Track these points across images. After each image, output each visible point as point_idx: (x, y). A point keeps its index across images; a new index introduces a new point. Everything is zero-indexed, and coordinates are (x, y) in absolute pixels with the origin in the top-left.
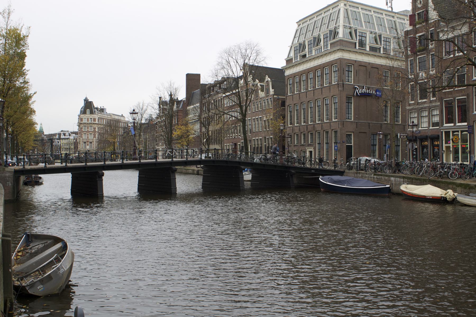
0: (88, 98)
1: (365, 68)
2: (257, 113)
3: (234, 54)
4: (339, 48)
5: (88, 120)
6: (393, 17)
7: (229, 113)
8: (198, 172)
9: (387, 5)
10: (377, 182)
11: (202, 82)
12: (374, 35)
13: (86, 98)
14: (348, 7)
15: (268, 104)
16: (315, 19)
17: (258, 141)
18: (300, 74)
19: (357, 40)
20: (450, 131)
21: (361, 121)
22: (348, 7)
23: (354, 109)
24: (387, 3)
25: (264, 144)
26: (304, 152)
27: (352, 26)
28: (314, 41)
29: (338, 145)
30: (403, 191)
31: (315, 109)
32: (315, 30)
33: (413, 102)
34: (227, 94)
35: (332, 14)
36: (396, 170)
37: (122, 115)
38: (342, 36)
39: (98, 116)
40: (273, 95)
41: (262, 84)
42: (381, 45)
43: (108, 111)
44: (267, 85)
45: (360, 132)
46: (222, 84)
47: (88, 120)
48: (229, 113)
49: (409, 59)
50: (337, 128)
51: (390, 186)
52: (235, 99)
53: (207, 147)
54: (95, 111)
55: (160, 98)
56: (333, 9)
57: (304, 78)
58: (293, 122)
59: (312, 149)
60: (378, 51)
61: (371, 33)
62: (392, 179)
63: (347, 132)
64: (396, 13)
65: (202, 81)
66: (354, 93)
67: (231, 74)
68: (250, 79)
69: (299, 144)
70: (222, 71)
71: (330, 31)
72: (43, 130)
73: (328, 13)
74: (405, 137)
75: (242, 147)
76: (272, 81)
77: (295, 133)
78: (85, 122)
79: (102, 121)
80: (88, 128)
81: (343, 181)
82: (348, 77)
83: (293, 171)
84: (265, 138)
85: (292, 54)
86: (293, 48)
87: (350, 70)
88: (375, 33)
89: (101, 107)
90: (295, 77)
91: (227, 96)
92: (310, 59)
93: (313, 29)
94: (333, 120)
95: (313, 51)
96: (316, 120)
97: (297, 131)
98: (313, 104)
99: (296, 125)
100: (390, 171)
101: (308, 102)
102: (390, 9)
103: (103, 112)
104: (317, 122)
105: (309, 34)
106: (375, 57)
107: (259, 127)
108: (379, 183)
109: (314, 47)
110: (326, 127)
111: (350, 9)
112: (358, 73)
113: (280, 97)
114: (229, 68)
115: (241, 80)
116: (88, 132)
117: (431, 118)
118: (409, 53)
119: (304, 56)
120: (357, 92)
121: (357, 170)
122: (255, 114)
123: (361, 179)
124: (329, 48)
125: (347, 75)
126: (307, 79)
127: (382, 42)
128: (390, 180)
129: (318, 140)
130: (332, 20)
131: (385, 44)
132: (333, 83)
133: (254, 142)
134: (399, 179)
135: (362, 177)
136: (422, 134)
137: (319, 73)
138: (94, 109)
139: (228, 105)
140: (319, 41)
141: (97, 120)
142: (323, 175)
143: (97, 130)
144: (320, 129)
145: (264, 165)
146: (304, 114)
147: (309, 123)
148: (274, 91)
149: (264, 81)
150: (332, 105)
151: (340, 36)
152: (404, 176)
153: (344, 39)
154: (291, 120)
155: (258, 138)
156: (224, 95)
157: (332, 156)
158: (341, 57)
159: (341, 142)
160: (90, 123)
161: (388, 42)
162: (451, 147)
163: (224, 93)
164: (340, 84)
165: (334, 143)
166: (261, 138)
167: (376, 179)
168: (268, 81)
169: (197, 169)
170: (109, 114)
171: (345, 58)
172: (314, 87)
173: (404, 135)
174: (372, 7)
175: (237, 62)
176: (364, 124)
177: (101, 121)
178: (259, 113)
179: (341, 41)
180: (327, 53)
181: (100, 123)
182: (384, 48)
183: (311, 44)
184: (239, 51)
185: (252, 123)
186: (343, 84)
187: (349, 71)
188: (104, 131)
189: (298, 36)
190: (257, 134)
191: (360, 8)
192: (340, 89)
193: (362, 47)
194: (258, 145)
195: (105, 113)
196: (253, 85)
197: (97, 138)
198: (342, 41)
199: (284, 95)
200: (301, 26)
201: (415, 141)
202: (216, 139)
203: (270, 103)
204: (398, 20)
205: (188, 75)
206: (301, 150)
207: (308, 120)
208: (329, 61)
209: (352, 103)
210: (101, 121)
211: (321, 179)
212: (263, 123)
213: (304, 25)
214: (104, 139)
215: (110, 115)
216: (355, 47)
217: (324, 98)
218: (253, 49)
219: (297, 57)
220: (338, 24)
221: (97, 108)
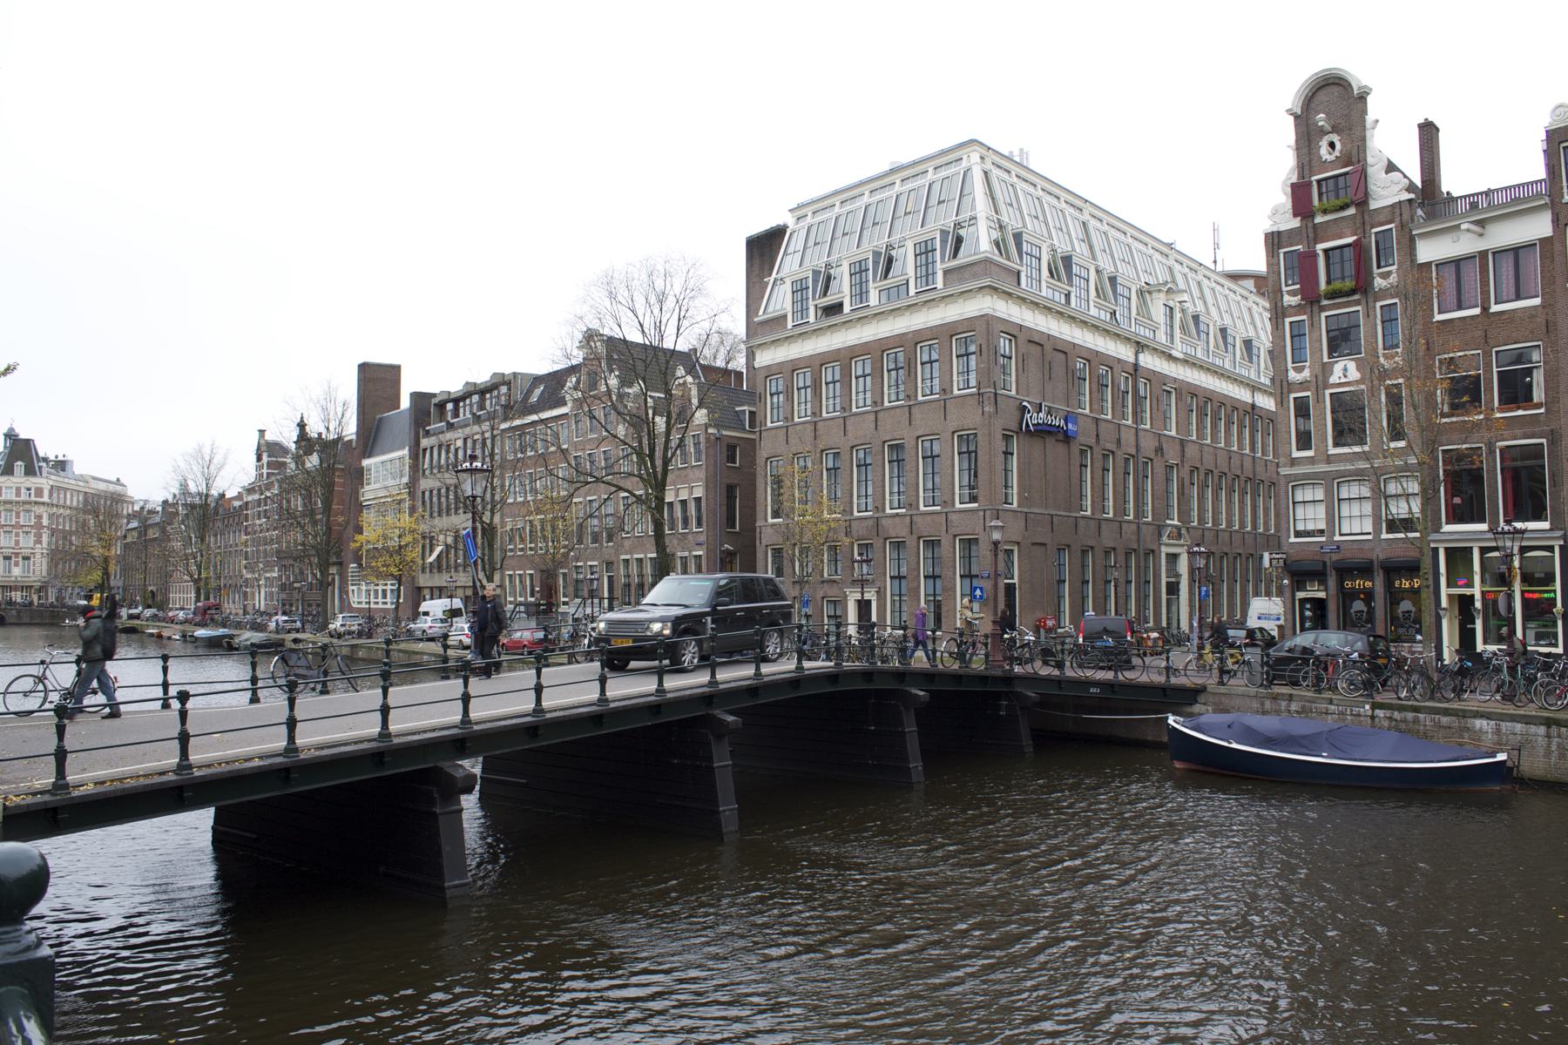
4: (986, 282)
5: (18, 493)
13: (12, 429)
18: (818, 363)
20: (1471, 548)
31: (880, 469)
37: (118, 480)
39: (51, 483)
40: (707, 426)
43: (79, 468)
47: (18, 493)
54: (40, 468)
55: (262, 432)
71: (942, 232)
74: (1281, 561)
79: (62, 496)
80: (18, 516)
81: (1304, 737)
89: (57, 457)
96: (884, 504)
103: (64, 470)
113: (725, 433)
116: (18, 526)
119: (836, 309)
124: (940, 285)
134: (1518, 727)
136: (1349, 555)
138: (38, 461)
143: (45, 522)
144: (904, 532)
152: (1548, 718)
155: (641, 556)
160: (25, 503)
162: (1478, 596)
170: (82, 476)
176: (1040, 517)
177: (59, 498)
181: (55, 502)
186: (996, 394)
188: (74, 526)
192: (987, 409)
195: (70, 475)
197: (45, 544)
201: (1319, 575)
205: (364, 368)
210: (59, 498)
214: (74, 548)
215: (82, 478)
221: (45, 460)
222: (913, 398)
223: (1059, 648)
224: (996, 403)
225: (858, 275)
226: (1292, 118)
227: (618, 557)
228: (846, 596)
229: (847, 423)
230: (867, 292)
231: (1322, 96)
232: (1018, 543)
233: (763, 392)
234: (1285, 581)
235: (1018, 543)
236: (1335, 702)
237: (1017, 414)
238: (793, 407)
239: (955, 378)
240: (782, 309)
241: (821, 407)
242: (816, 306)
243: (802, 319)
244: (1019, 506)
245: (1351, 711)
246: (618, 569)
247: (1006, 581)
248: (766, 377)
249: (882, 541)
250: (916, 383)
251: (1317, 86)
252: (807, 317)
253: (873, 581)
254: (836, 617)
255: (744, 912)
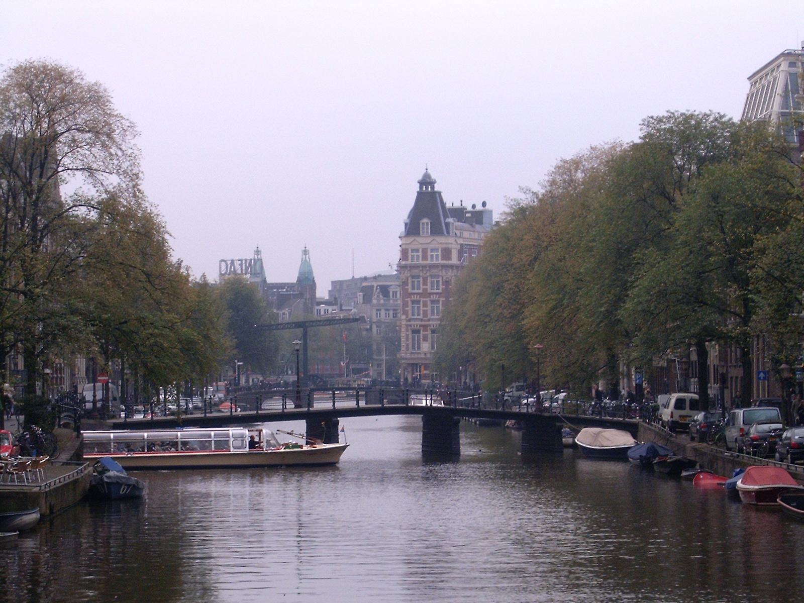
0: (433, 177)
5: (425, 257)
39: (460, 241)
47: (425, 257)
54: (447, 225)
72: (310, 272)
78: (415, 262)
89: (474, 206)
141: (454, 254)
223: (786, 293)
255: (682, 576)
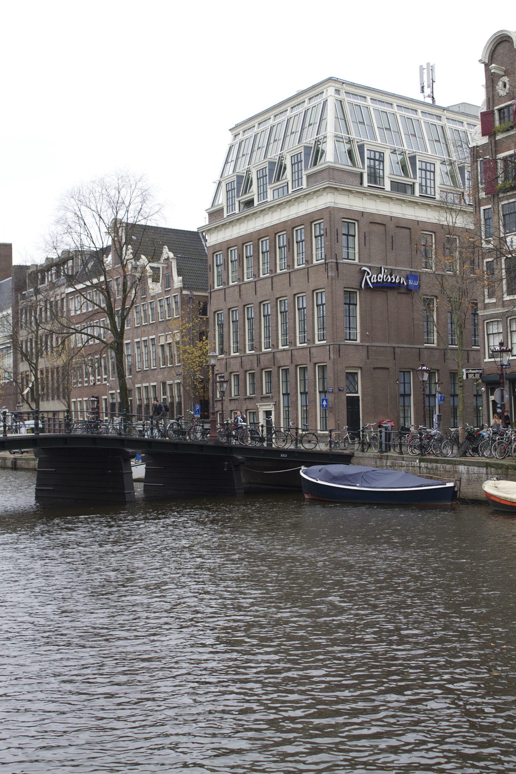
1: (382, 227)
2: (145, 329)
3: (92, 199)
4: (326, 184)
6: (439, 117)
7: (83, 331)
8: (15, 462)
9: (423, 91)
10: (427, 477)
11: (13, 265)
12: (400, 157)
14: (342, 96)
15: (169, 310)
16: (271, 122)
17: (147, 392)
18: (224, 247)
19: (364, 168)
21: (378, 344)
22: (342, 96)
23: (361, 318)
24: (423, 88)
25: (163, 397)
26: (254, 413)
27: (353, 136)
28: (271, 170)
29: (330, 397)
30: (488, 495)
31: (275, 318)
32: (271, 146)
33: (494, 300)
34: (80, 286)
35: (310, 111)
36: (467, 448)
38: (332, 160)
40: (181, 289)
41: (155, 265)
42: (415, 178)
44: (167, 268)
45: (374, 368)
46: (48, 271)
48: (83, 331)
49: (482, 208)
50: (327, 360)
51: (455, 484)
52: (100, 299)
53: (34, 406)
56: (310, 99)
57: (249, 251)
58: (225, 349)
59: (271, 407)
60: (409, 191)
61: (394, 152)
62: (462, 468)
63: (347, 367)
64: (444, 109)
65: (17, 260)
66: (361, 283)
67: (87, 242)
68: (128, 253)
69: (242, 397)
70: (68, 239)
71: (306, 148)
73: (301, 109)
74: (477, 376)
75: (113, 405)
76: (178, 259)
77: (231, 373)
81: (350, 475)
82: (348, 248)
83: (240, 457)
84: (164, 384)
85: (222, 200)
86: (223, 185)
87: (351, 233)
88: (403, 153)
90: (228, 248)
91: (80, 291)
92: (262, 211)
93: (268, 145)
94: (317, 342)
95: (270, 193)
97: (235, 367)
98: (271, 308)
99: (232, 354)
100: (455, 451)
101: (260, 303)
102: (429, 101)
104: (281, 347)
105: (258, 156)
106: (404, 205)
107: (149, 360)
108: (431, 478)
109: (270, 183)
110: (301, 359)
111: (348, 99)
112: (367, 238)
113: (195, 293)
114: (82, 231)
115: (107, 257)
117: (509, 337)
118: (482, 195)
119: (249, 203)
120: (366, 279)
121: (381, 452)
122: (139, 331)
123: (390, 471)
124: (304, 186)
125: (345, 244)
126: (256, 254)
127: (418, 171)
128: (456, 472)
129: (285, 386)
130: (310, 125)
131: (424, 176)
132: (315, 262)
133: (140, 393)
135: (393, 466)
137: (283, 240)
139: (84, 311)
140: (282, 169)
142: (308, 464)
144: (288, 362)
145: (175, 445)
146: (251, 329)
147: (263, 350)
148: (183, 281)
149: (159, 259)
150: (313, 310)
151: (328, 159)
152: (487, 463)
153: (337, 165)
154: (222, 343)
155: (147, 384)
156: (71, 290)
157: (316, 421)
158: (332, 205)
159: (336, 390)
161: (430, 171)
163: (71, 285)
164: (329, 265)
165: (320, 392)
166: (155, 384)
167: (425, 471)
168: (168, 259)
169: (12, 456)
171: (340, 206)
172: (273, 270)
173: (476, 371)
174: (393, 95)
175: (100, 217)
176: (382, 349)
178: (150, 328)
179: (330, 170)
180: (299, 197)
182: (421, 185)
183: (263, 177)
184: (104, 192)
185: (133, 351)
186: (337, 263)
187: (348, 235)
189: (234, 158)
190: (145, 374)
191: (368, 98)
192: (330, 274)
193: (375, 183)
194: (148, 399)
196: (135, 268)
198: (334, 169)
199: (205, 290)
200: (240, 137)
202: (58, 388)
203: (174, 307)
204: (449, 125)
205: (10, 245)
206: (246, 410)
207: (260, 342)
208: (304, 213)
209: (356, 305)
211: (305, 473)
212: (160, 350)
213: (247, 135)
216: (361, 183)
217: (295, 295)
218: (133, 186)
219: (233, 204)
220: (322, 134)
222: (291, 267)
224: (337, 269)
225: (262, 179)
226: (483, 65)
227: (135, 386)
228: (258, 409)
229: (257, 286)
230: (266, 191)
231: (500, 50)
232: (361, 368)
233: (211, 264)
234: (483, 389)
235: (361, 368)
236: (405, 459)
237: (358, 276)
238: (228, 275)
239: (314, 252)
240: (222, 204)
241: (243, 274)
242: (239, 201)
243: (298, 186)
244: (361, 342)
245: (411, 464)
246: (135, 395)
247: (348, 395)
248: (214, 253)
249: (276, 369)
250: (293, 257)
251: (497, 43)
252: (267, 198)
253: (272, 397)
254: (254, 423)
